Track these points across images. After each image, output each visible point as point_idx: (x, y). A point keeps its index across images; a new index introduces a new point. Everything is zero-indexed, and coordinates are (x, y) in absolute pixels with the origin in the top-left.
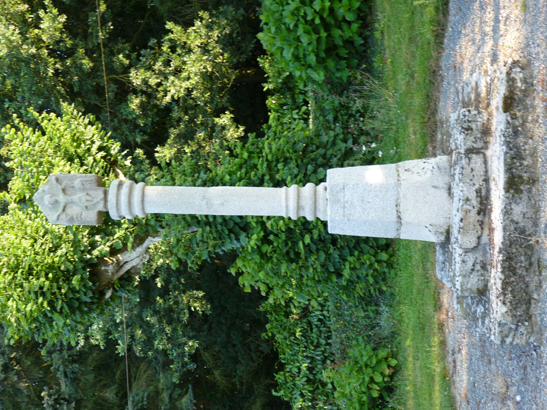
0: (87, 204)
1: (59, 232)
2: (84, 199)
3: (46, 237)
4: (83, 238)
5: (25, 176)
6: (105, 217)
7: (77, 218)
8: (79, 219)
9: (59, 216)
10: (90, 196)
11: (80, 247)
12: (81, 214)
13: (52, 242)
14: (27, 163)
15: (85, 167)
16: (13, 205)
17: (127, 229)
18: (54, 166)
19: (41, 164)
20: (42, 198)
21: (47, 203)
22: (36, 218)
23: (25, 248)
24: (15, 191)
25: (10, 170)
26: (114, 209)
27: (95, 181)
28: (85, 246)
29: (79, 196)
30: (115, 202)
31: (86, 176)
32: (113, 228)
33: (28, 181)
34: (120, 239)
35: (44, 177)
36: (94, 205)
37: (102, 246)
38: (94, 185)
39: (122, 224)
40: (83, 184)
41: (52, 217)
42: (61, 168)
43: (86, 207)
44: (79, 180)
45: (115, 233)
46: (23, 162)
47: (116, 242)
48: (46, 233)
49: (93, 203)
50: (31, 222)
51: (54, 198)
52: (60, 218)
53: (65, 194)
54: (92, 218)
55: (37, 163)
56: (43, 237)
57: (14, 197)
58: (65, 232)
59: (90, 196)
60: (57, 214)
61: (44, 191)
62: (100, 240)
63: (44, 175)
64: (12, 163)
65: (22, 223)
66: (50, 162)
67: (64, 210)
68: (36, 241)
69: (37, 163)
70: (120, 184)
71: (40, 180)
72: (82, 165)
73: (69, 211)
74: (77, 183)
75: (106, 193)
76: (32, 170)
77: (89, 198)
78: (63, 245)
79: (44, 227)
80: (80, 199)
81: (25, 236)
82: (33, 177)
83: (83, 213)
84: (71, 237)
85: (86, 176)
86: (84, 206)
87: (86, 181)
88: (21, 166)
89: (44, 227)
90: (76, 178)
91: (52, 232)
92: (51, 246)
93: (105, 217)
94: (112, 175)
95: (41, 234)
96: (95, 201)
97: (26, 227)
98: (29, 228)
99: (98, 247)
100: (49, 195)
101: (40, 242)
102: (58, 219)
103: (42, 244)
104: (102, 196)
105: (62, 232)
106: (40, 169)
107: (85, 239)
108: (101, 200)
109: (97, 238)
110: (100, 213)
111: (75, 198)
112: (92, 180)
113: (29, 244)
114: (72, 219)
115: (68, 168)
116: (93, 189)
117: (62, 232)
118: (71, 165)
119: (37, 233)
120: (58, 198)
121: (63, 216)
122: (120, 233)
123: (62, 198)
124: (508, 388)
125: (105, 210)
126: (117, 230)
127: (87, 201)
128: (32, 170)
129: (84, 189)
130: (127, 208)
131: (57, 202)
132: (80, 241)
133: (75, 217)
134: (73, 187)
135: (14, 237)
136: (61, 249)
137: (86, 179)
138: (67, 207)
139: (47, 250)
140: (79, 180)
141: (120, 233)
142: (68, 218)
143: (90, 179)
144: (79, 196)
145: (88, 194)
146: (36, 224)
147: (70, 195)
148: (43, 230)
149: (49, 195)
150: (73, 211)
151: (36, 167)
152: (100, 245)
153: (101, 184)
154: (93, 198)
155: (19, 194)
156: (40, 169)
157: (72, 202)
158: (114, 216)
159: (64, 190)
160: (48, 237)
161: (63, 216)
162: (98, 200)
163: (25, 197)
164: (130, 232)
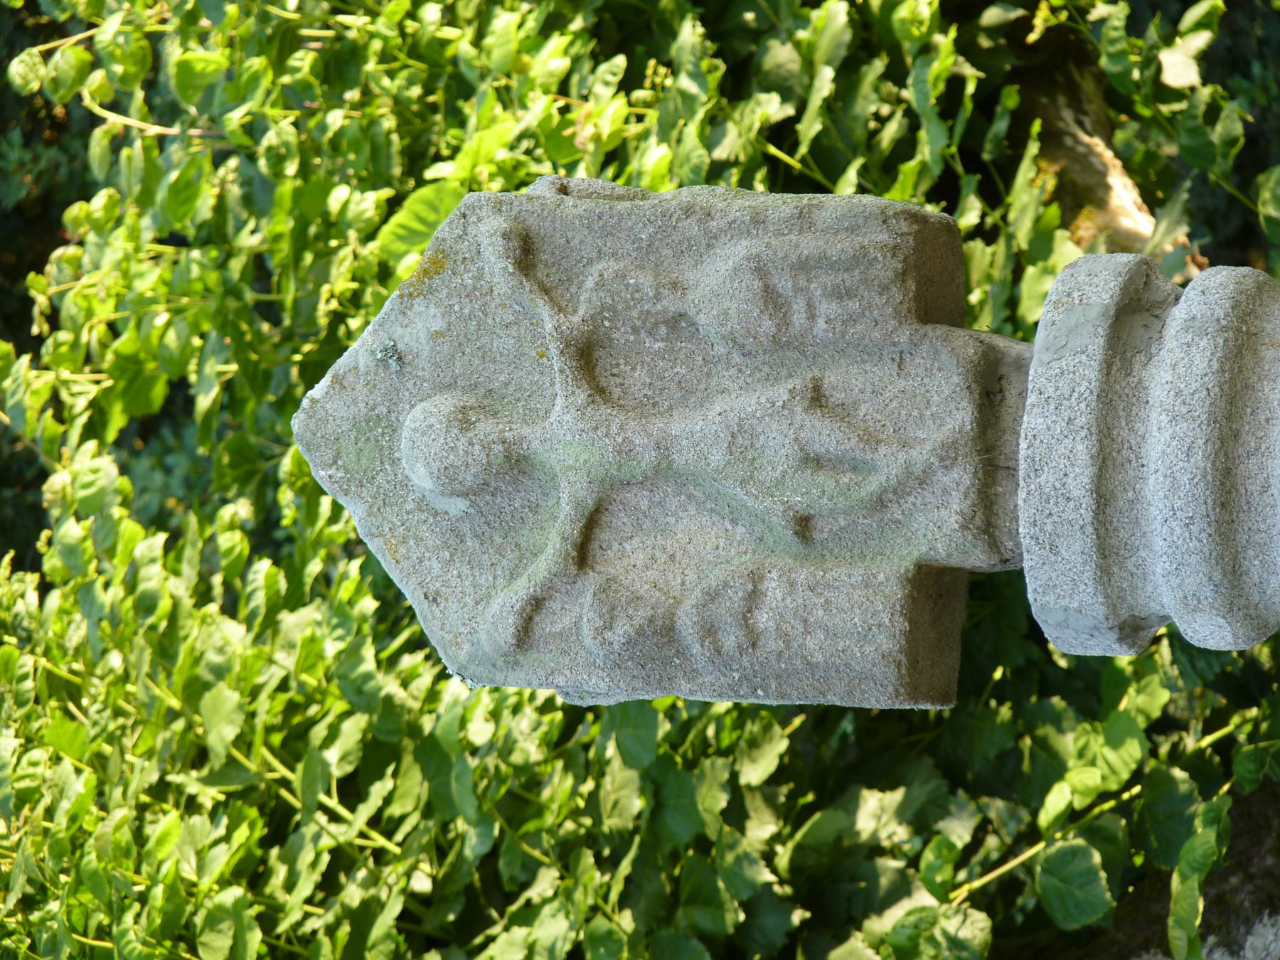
0: (808, 492)
1: (505, 747)
2: (778, 447)
3: (379, 790)
4: (736, 815)
5: (185, 191)
6: (975, 615)
7: (709, 631)
8: (730, 640)
9: (537, 604)
10: (844, 414)
11: (713, 902)
12: (754, 597)
13: (440, 850)
14: (210, 58)
15: (770, 107)
16: (84, 470)
17: (1165, 724)
18: (463, 88)
19: (340, 65)
20: (379, 428)
21: (421, 478)
22: (294, 600)
23: (183, 891)
24: (93, 335)
25: (57, 127)
26: (1077, 549)
27: (886, 268)
28: (756, 901)
29: (730, 418)
30: (1080, 482)
31: (803, 219)
32: (1026, 721)
33: (215, 234)
34: (1094, 834)
35: (368, 203)
36: (879, 503)
37: (923, 898)
38: (882, 309)
39: (1120, 683)
40: (771, 299)
41: (467, 606)
42: (540, 107)
43: (803, 526)
44: (735, 252)
45: (1055, 769)
46: (174, 53)
47: (1055, 864)
48: (377, 756)
49: (873, 485)
50: (234, 634)
51: (486, 427)
52: (546, 625)
53: (599, 392)
54: (849, 634)
55: (303, 61)
56: (352, 791)
57: (82, 390)
58: (558, 744)
59: (844, 414)
60: (522, 589)
61: (395, 355)
62: (900, 833)
63: (368, 183)
64: (68, 53)
65: (165, 647)
66: (427, 53)
67: (583, 553)
68: (281, 827)
69: (303, 61)
70: (1136, 310)
71: (334, 226)
72: (739, 82)
73: (630, 558)
74: (716, 284)
75: (992, 388)
76: (255, 128)
77: (824, 435)
78: (546, 882)
79: (360, 697)
80: (741, 439)
81: (190, 782)
82: (257, 197)
83: (773, 587)
84: (625, 799)
85: (803, 219)
86: (775, 510)
87: (803, 266)
88: (151, 86)
89: (360, 697)
90: (712, 240)
91: (436, 756)
92: (422, 884)
93: (975, 615)
94: (1031, 186)
95: (337, 760)
96: (889, 464)
97: (194, 691)
98: (227, 696)
99: (880, 907)
100: (446, 403)
101: (322, 836)
102: (525, 635)
103: (342, 860)
104: (962, 416)
105: (530, 750)
106: (336, 119)
107: (761, 828)
108: (948, 453)
109: (876, 814)
110: (930, 583)
111: (696, 430)
112: (860, 258)
113: (222, 859)
114: (658, 642)
115: (604, 112)
116: (868, 352)
117: (530, 750)
118: (629, 83)
119: (294, 744)
120: (532, 436)
121: (577, 612)
122: (1091, 766)
123: (565, 435)
124: (139, 837)
125: (978, 559)
126: (1068, 743)
127: (812, 461)
128: (255, 128)
129: (778, 346)
130: (1197, 542)
131: (516, 464)
132: (703, 844)
133: (687, 623)
134: (677, 323)
135: (81, 785)
136: (529, 915)
137: (808, 245)
138: (618, 519)
139: (385, 922)
140: (735, 252)
141: (1091, 766)
142: (623, 629)
143: (841, 246)
144: (730, 418)
145: (817, 398)
146: (286, 661)
147: (648, 407)
148: (354, 728)
149: (446, 403)
150: (680, 557)
151: (292, 97)
152: (902, 889)
153: (935, 292)
154: (871, 439)
155: (129, 367)
156: (336, 119)
157: (664, 472)
158: (1069, 617)
159: (586, 356)
160: (402, 789)
161: (577, 612)
162: (920, 455)
163: (181, 392)
164: (1195, 764)
